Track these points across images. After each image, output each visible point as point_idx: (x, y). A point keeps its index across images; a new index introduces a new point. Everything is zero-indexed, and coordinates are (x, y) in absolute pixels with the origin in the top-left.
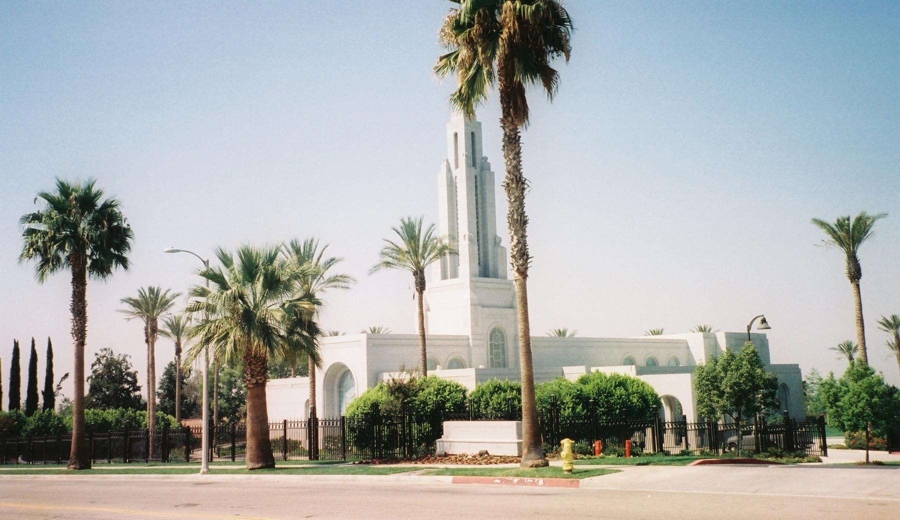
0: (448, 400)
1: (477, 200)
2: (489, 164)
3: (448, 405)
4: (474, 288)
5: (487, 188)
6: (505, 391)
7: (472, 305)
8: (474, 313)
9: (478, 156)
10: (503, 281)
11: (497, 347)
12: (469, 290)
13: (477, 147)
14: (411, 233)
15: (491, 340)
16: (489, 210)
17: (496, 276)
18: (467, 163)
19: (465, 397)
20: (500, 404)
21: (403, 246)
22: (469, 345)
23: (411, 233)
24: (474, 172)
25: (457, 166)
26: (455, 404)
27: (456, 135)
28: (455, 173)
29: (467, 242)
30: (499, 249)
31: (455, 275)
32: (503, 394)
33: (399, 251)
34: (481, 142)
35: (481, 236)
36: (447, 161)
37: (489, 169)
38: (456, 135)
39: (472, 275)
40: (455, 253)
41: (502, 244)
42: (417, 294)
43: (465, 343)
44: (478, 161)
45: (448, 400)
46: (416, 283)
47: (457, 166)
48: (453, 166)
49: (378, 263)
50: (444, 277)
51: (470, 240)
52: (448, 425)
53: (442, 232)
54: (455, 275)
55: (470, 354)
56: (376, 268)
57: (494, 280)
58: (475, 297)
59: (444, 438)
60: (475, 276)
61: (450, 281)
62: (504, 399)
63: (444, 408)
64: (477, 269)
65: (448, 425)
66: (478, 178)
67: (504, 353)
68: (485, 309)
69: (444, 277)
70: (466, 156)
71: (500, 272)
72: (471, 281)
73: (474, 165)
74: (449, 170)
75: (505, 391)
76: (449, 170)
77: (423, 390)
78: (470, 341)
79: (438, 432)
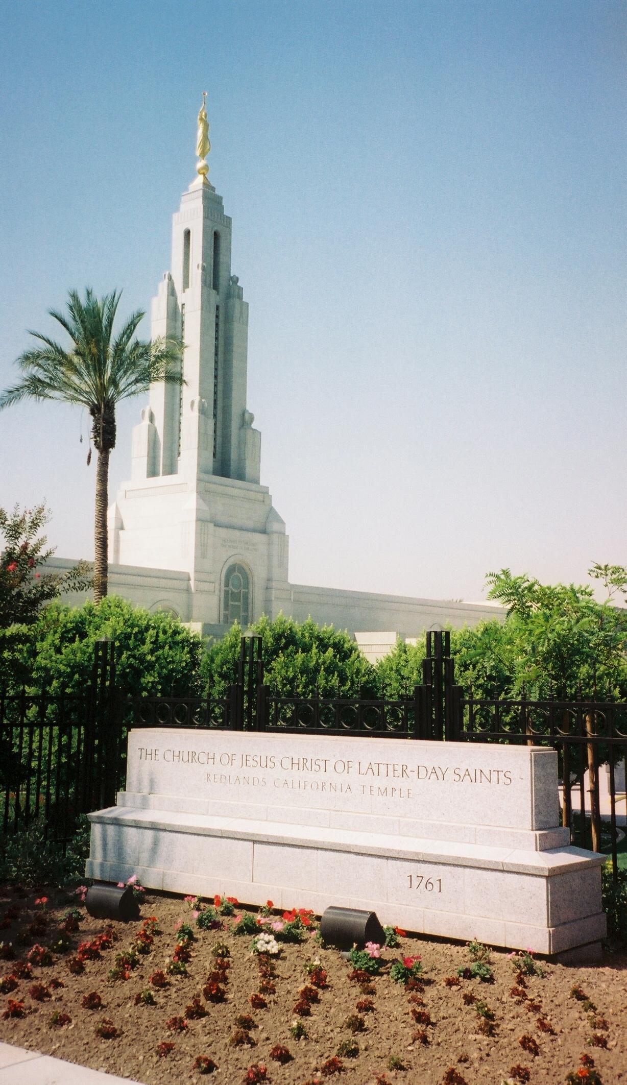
0: (150, 666)
1: (217, 347)
2: (241, 289)
3: (148, 679)
4: (203, 493)
5: (236, 327)
6: (306, 649)
7: (198, 520)
8: (201, 534)
9: (222, 273)
10: (253, 486)
11: (235, 597)
12: (194, 496)
13: (222, 259)
14: (91, 324)
15: (227, 585)
16: (235, 363)
17: (241, 477)
18: (204, 283)
19: (194, 663)
20: (291, 681)
21: (68, 345)
22: (188, 590)
23: (91, 324)
24: (215, 298)
25: (186, 284)
26: (166, 679)
27: (187, 234)
28: (181, 298)
29: (196, 413)
30: (249, 432)
31: (171, 469)
32: (300, 657)
33: (59, 357)
34: (229, 249)
35: (220, 406)
36: (170, 278)
37: (240, 297)
38: (187, 234)
39: (202, 470)
40: (175, 379)
41: (254, 426)
42: (96, 454)
43: (183, 585)
44: (223, 282)
45: (150, 666)
46: (96, 429)
47: (186, 284)
48: (178, 286)
49: (18, 382)
50: (153, 472)
51: (202, 411)
52: (141, 741)
53: (154, 330)
54: (171, 469)
55: (189, 606)
56: (14, 394)
57: (239, 483)
58: (205, 507)
59: (126, 807)
60: (206, 472)
61: (162, 480)
62: (304, 670)
63: (136, 688)
64: (210, 462)
65: (141, 741)
66: (221, 310)
67: (246, 610)
68: (220, 529)
69: (153, 472)
70: (204, 269)
71: (249, 471)
72: (199, 480)
73: (216, 287)
74: (172, 292)
75: (306, 649)
76: (172, 292)
77: (83, 635)
78: (192, 583)
79: (104, 777)
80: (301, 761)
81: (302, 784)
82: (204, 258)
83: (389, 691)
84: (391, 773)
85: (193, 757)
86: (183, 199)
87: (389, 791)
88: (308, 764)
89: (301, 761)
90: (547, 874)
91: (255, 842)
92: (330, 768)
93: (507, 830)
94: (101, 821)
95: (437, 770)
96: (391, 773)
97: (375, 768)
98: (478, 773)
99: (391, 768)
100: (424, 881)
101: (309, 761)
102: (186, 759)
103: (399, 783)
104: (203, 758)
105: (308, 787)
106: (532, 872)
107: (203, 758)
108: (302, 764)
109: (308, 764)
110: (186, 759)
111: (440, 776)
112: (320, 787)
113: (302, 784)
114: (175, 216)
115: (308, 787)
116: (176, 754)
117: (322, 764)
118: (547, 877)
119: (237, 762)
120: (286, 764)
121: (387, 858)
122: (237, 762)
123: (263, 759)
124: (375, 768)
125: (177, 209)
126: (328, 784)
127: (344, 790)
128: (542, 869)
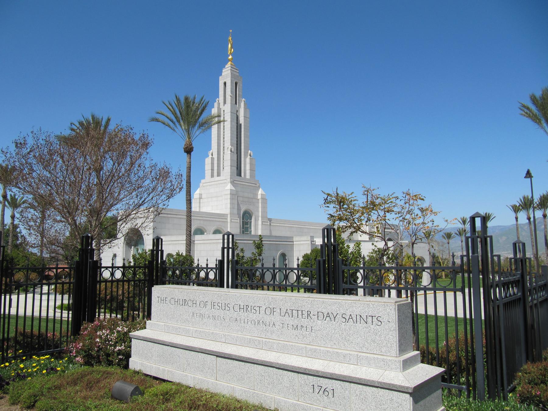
25: (225, 102)
27: (225, 83)
38: (225, 83)
47: (225, 102)
61: (216, 178)
80: (245, 306)
81: (246, 321)
82: (232, 92)
83: (22, 281)
84: (300, 316)
85: (462, 242)
86: (223, 71)
87: (299, 327)
88: (249, 309)
89: (245, 306)
90: (410, 391)
91: (217, 356)
92: (262, 312)
93: (379, 357)
94: (138, 338)
95: (331, 315)
96: (300, 316)
97: (290, 312)
98: (358, 317)
99: (300, 313)
100: (323, 389)
101: (250, 307)
102: (181, 303)
103: (305, 322)
104: (190, 303)
105: (249, 323)
106: (399, 389)
107: (190, 303)
108: (246, 308)
109: (249, 309)
110: (181, 303)
111: (333, 319)
112: (257, 324)
113: (246, 321)
114: (220, 77)
115: (249, 323)
116: (176, 300)
117: (257, 309)
118: (411, 394)
119: (209, 307)
120: (237, 308)
121: (298, 373)
122: (209, 307)
123: (223, 304)
124: (290, 312)
125: (221, 75)
126: (261, 322)
127: (271, 326)
128: (408, 388)
